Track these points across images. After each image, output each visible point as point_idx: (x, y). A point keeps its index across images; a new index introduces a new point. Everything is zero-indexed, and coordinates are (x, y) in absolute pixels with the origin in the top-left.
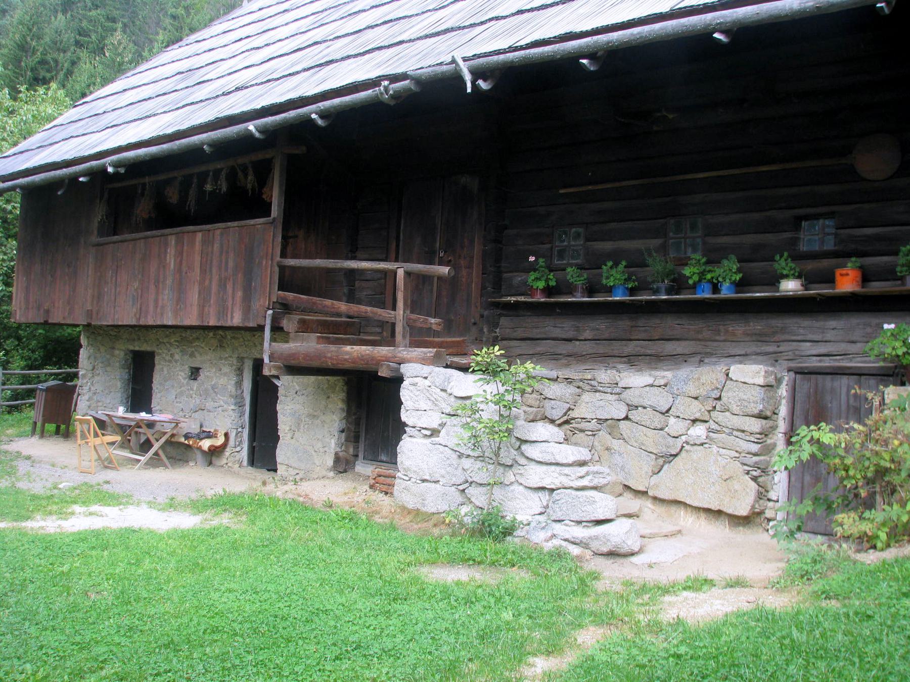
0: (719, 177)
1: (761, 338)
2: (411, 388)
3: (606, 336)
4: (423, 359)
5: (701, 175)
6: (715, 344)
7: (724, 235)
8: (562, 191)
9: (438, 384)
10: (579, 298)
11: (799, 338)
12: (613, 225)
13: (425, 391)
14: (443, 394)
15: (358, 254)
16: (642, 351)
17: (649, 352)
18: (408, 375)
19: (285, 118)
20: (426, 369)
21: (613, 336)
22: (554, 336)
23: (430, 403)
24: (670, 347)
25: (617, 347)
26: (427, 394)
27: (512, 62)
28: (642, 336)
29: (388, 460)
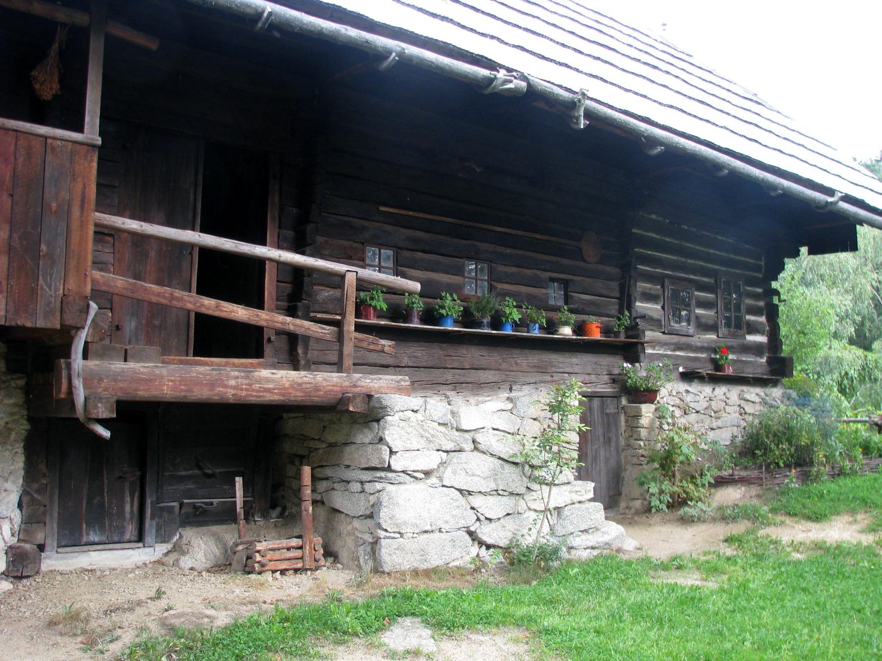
0: (506, 233)
1: (542, 369)
2: (402, 424)
3: (424, 364)
4: (399, 389)
5: (499, 229)
6: (513, 373)
7: (506, 283)
8: (382, 209)
9: (436, 418)
10: (416, 324)
11: (561, 370)
12: (420, 255)
13: (418, 427)
14: (442, 429)
15: (308, 249)
16: (462, 379)
17: (470, 380)
18: (397, 408)
19: (338, 31)
20: (415, 401)
21: (430, 364)
22: (372, 361)
23: (422, 441)
24: (484, 376)
25: (436, 374)
26: (421, 431)
27: (615, 120)
28: (456, 365)
29: (104, 538)
